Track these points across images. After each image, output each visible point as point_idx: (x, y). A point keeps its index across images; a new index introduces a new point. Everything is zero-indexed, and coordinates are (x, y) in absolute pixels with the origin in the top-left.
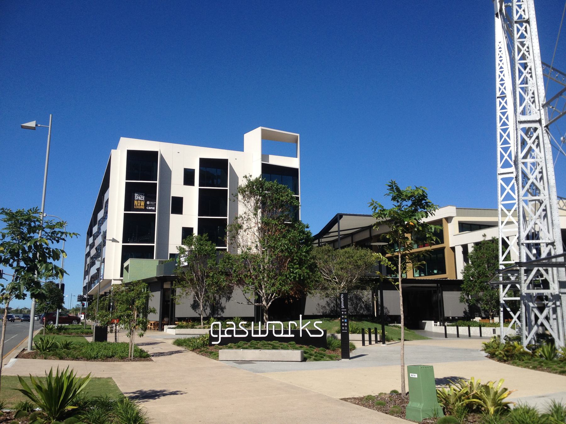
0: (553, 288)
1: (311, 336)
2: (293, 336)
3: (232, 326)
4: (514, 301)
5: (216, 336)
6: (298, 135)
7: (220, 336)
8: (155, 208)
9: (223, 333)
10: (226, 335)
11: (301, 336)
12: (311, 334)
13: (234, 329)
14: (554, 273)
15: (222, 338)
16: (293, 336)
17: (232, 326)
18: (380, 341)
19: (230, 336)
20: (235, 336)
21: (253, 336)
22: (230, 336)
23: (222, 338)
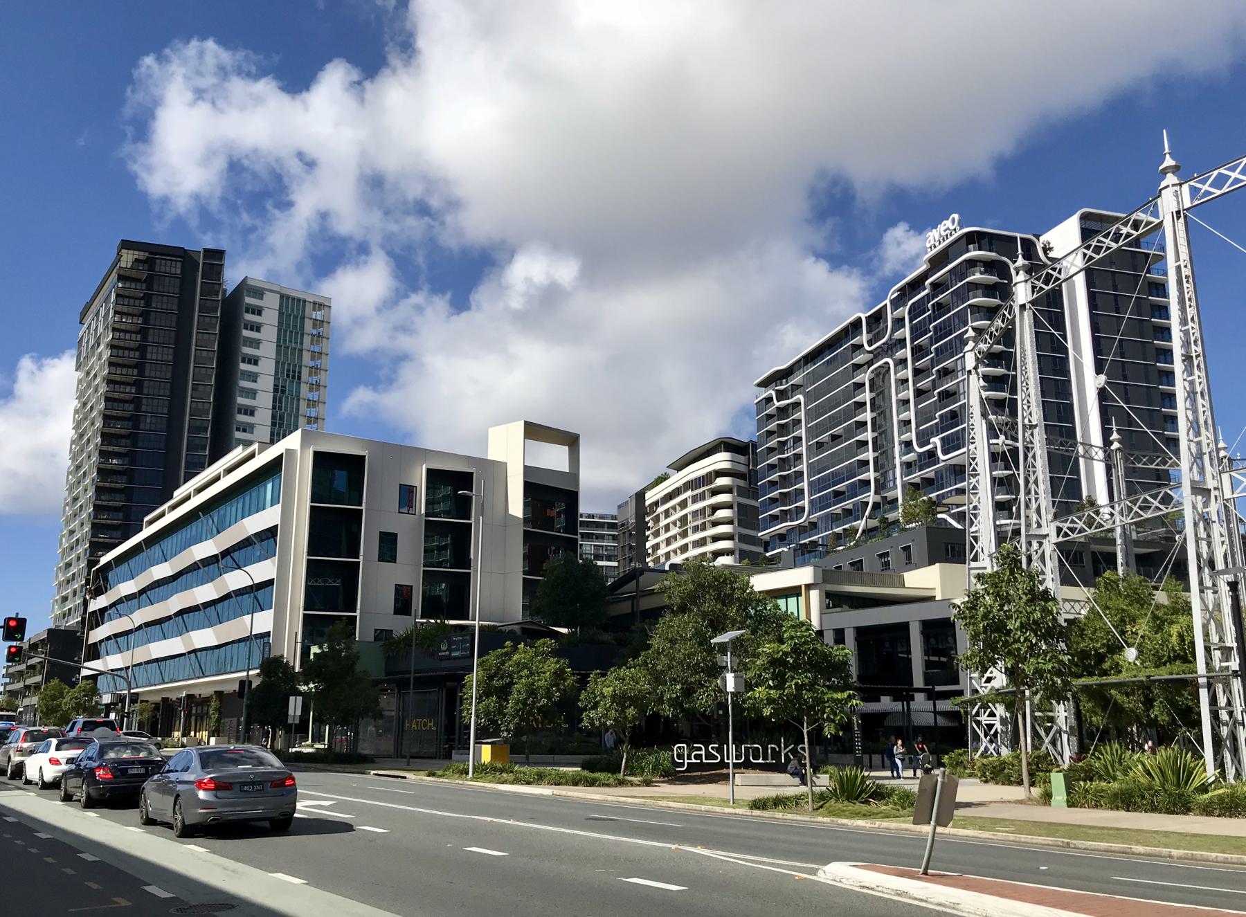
3: (700, 749)
5: (682, 761)
7: (686, 761)
9: (689, 758)
13: (703, 752)
17: (700, 749)
20: (704, 761)
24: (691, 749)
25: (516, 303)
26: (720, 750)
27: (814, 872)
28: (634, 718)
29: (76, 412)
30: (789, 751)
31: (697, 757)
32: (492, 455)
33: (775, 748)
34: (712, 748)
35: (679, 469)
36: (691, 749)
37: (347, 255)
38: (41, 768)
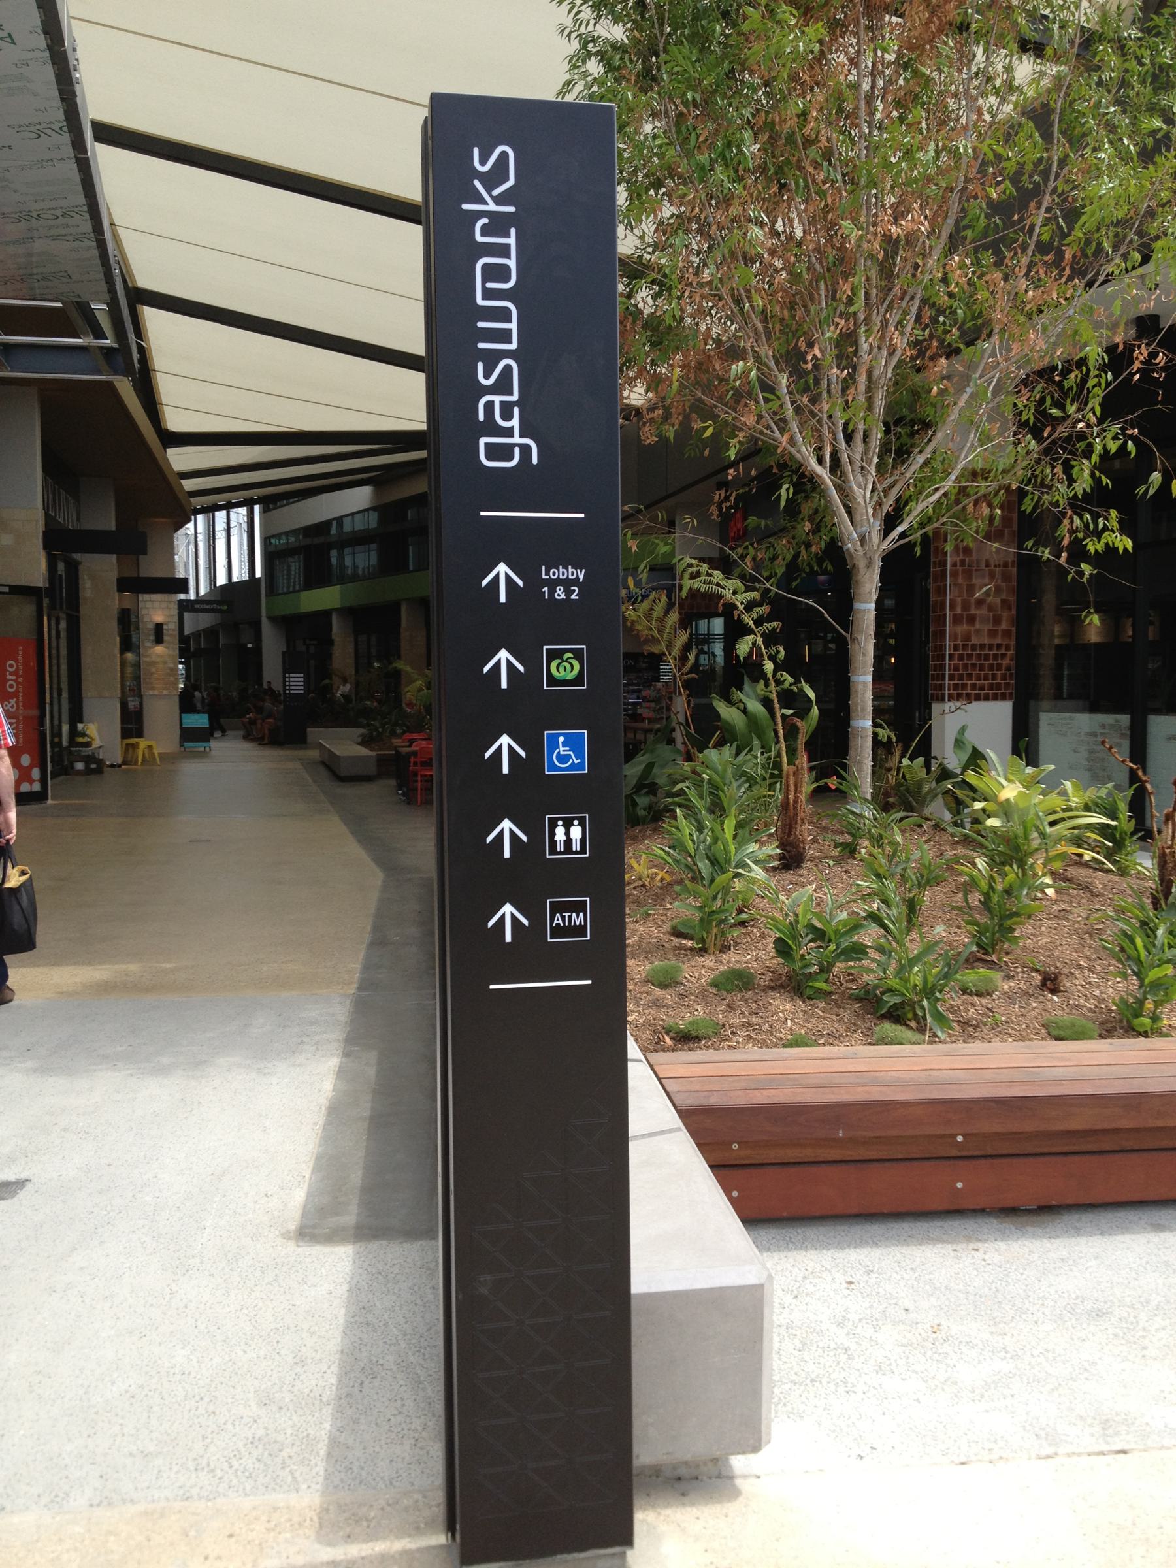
0: (205, 1061)
1: (511, 182)
2: (513, 231)
3: (489, 406)
4: (889, 603)
5: (517, 451)
6: (588, 938)
7: (517, 439)
8: (561, 853)
9: (509, 432)
10: (515, 423)
11: (589, 982)
12: (507, 179)
13: (497, 399)
14: (838, 1158)
15: (521, 436)
16: (513, 231)
17: (489, 406)
18: (1071, 697)
19: (516, 410)
20: (515, 397)
21: (514, 346)
22: (516, 410)
23: (521, 436)
24: (491, 428)
25: (741, 435)
26: (491, 359)
27: (61, 576)
28: (631, 382)
29: (1002, 1040)
30: (489, 192)
31: (507, 416)
32: (644, 1519)
33: (483, 227)
34: (487, 376)
35: (865, 432)
36: (491, 428)
37: (1039, 61)
38: (759, 1477)
